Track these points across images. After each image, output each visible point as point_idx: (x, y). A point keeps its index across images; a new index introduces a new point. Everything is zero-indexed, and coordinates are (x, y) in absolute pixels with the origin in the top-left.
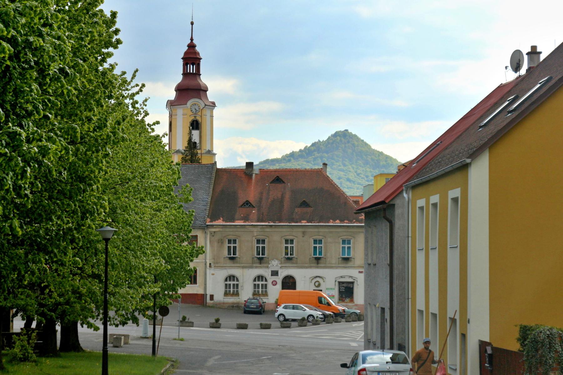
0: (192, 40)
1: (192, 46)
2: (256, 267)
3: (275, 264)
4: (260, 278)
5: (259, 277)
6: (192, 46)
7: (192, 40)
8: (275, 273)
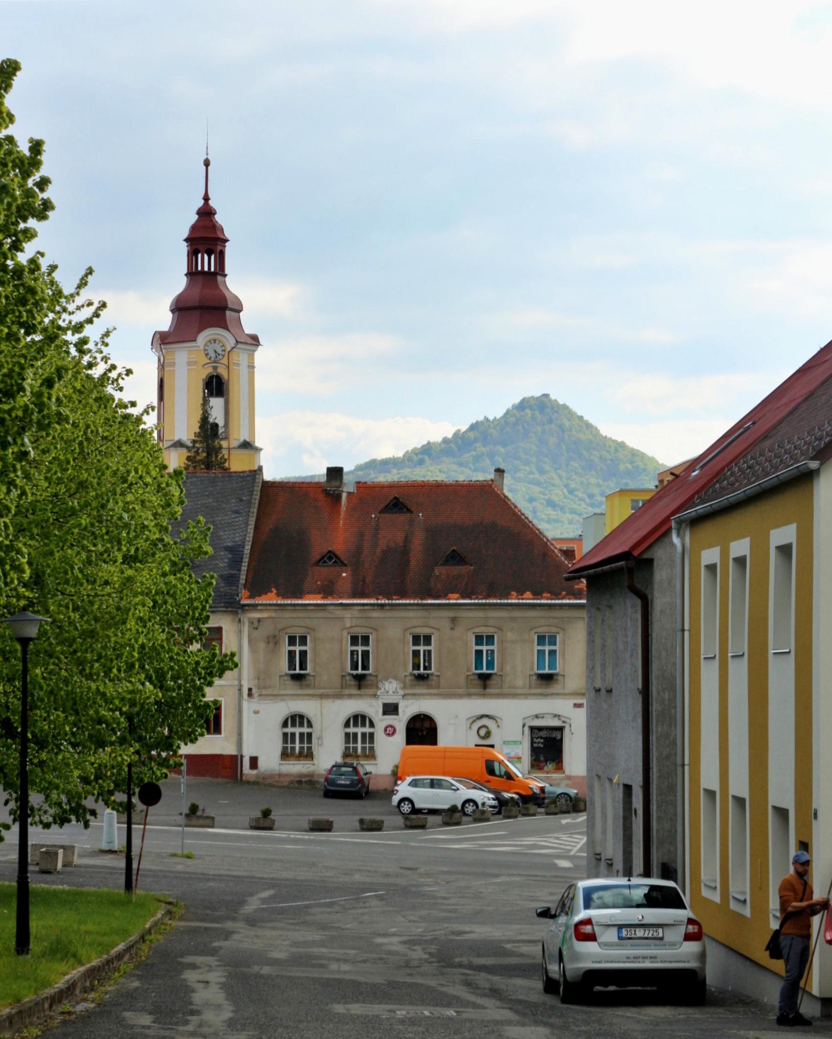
0: (206, 198)
1: (206, 213)
2: (350, 696)
3: (390, 690)
4: (359, 719)
5: (356, 717)
6: (206, 213)
7: (206, 198)
8: (391, 709)
